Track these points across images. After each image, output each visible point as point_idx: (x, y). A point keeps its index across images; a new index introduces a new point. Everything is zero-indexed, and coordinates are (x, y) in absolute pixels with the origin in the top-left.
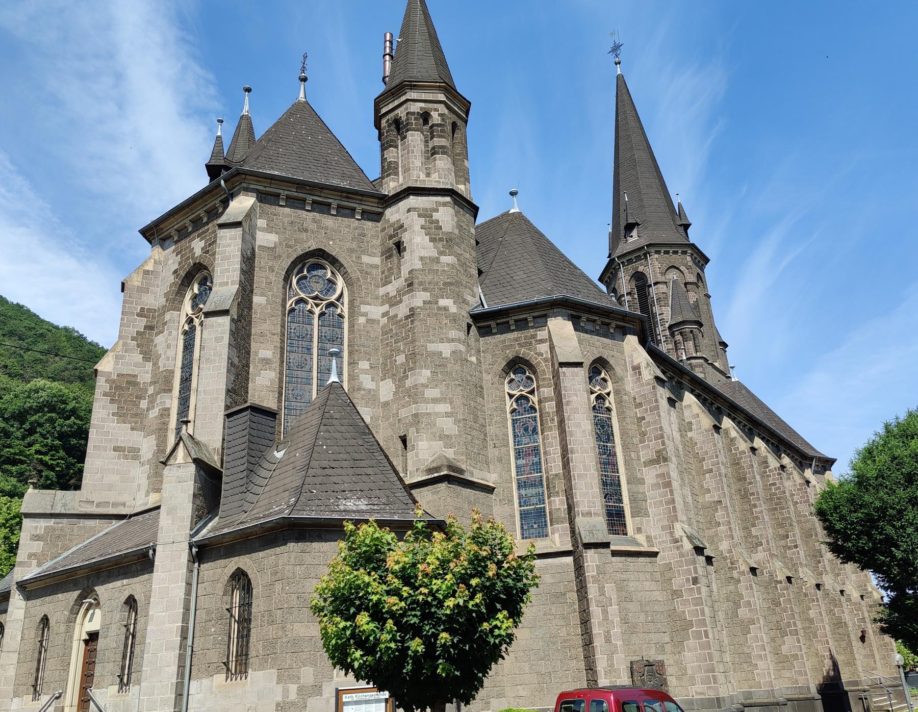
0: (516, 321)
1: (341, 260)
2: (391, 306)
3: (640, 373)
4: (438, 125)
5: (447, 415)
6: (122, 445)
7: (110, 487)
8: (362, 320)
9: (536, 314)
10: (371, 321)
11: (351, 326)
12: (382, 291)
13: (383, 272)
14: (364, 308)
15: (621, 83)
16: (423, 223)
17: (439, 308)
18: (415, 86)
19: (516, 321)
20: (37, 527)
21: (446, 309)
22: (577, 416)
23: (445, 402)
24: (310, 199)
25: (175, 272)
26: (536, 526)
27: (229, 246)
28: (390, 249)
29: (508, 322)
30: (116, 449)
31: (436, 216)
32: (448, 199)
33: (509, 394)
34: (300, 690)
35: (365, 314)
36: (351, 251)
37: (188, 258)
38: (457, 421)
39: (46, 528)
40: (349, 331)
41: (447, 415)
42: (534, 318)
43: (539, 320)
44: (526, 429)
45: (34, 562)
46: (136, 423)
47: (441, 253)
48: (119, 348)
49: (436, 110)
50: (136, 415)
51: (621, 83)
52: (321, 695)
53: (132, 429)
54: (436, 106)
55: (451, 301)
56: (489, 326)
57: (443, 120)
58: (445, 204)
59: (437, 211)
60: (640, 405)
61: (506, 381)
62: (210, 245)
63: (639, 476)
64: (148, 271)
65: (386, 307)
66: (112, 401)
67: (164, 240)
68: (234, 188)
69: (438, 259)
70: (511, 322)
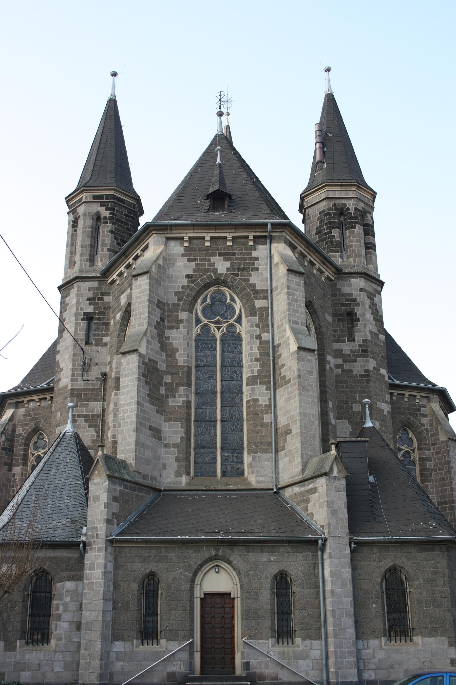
0: (410, 395)
9: (423, 395)
12: (335, 346)
18: (360, 188)
21: (383, 376)
25: (188, 276)
27: (296, 290)
28: (341, 315)
30: (151, 428)
37: (208, 270)
39: (120, 490)
45: (115, 521)
66: (147, 383)
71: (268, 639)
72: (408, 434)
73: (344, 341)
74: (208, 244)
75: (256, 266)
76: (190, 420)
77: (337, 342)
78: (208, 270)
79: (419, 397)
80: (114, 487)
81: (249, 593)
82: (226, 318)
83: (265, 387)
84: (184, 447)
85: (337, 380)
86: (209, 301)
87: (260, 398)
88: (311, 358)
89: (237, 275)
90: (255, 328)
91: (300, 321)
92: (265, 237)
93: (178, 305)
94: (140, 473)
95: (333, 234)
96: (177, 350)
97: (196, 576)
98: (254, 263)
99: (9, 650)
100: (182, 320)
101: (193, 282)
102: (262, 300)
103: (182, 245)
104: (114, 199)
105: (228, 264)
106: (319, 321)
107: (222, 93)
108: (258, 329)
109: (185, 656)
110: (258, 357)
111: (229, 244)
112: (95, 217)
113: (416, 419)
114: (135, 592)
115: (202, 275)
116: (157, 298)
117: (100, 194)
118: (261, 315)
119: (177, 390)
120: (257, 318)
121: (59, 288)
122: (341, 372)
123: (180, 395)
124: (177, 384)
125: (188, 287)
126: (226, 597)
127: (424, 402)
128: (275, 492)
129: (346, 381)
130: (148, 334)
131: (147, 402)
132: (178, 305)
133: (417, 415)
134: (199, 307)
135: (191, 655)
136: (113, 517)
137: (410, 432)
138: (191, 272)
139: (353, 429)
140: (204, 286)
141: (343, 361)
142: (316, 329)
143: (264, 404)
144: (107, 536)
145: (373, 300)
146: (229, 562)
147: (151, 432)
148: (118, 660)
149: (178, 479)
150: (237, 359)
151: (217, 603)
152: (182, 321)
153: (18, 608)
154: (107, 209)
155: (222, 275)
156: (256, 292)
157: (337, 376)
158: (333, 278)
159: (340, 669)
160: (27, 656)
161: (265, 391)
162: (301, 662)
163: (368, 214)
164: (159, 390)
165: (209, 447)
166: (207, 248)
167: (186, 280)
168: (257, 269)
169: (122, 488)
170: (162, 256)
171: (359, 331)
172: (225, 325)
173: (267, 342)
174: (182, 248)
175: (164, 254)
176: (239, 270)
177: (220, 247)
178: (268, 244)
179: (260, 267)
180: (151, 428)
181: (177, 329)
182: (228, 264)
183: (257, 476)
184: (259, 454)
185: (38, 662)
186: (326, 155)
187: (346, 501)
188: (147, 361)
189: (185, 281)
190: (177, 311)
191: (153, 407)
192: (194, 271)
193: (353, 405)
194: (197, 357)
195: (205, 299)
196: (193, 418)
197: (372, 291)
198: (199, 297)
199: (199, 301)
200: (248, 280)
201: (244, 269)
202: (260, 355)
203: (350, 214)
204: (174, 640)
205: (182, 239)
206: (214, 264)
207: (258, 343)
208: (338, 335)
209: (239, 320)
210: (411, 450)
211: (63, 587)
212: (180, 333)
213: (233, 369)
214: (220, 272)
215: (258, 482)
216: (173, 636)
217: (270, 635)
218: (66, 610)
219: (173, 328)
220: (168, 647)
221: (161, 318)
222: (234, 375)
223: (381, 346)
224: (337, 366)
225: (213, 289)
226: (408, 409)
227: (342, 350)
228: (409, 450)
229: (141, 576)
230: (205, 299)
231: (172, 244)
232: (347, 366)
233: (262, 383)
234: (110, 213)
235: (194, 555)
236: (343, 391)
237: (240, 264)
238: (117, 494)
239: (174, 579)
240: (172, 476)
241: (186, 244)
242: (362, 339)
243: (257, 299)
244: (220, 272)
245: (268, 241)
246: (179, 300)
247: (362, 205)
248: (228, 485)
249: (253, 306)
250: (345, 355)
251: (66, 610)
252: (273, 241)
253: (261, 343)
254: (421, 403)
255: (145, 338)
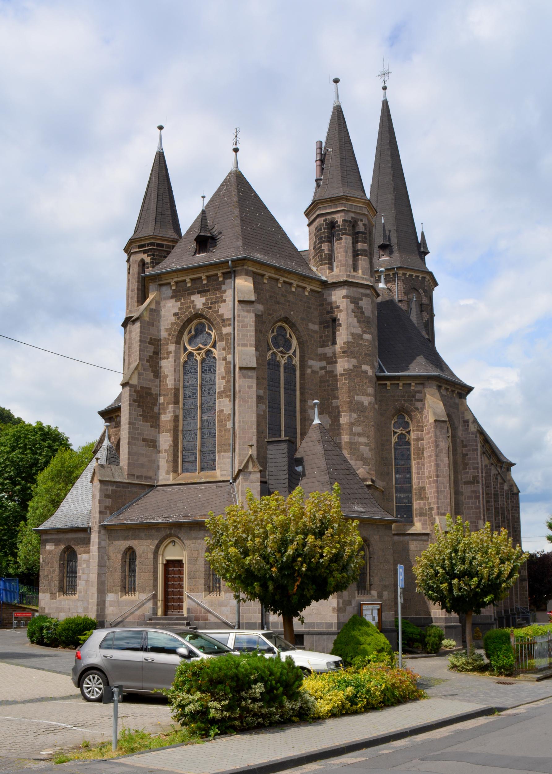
0: (403, 384)
1: (297, 325)
2: (328, 363)
3: (468, 426)
4: (362, 233)
5: (366, 444)
6: (147, 438)
7: (142, 466)
8: (309, 371)
9: (417, 382)
10: (313, 372)
11: (302, 375)
12: (320, 351)
13: (321, 337)
14: (311, 362)
15: (385, 104)
16: (353, 308)
17: (362, 372)
18: (349, 199)
19: (403, 384)
20: (107, 489)
21: (366, 372)
22: (442, 454)
23: (364, 437)
24: (282, 279)
25: (175, 314)
26: (405, 516)
27: (246, 317)
28: (327, 322)
29: (398, 384)
30: (144, 440)
31: (361, 303)
32: (368, 292)
33: (393, 431)
34: (344, 602)
35: (311, 367)
36: (303, 319)
37: (189, 307)
38: (371, 450)
39: (112, 490)
40: (300, 378)
41: (366, 444)
42: (416, 384)
43: (418, 386)
44: (403, 455)
45: (108, 512)
46: (153, 422)
47: (364, 332)
48: (140, 368)
49: (362, 221)
50: (152, 417)
51: (385, 104)
52: (351, 605)
53: (152, 427)
54: (361, 217)
55: (369, 367)
56: (386, 384)
57: (366, 229)
58: (366, 295)
59: (361, 300)
60: (466, 446)
61: (393, 422)
62: (211, 303)
63: (461, 490)
64: (152, 309)
65: (323, 364)
66: (139, 406)
67: (161, 285)
68: (236, 267)
69: (362, 336)
70: (401, 384)
71: (202, 592)
72: (405, 418)
73: (328, 346)
74: (189, 285)
75: (224, 298)
76: (178, 430)
77: (322, 347)
78: (189, 307)
79: (413, 384)
80: (106, 488)
81: (193, 560)
82: (206, 345)
83: (228, 399)
84: (172, 451)
85: (320, 381)
86: (193, 332)
87: (224, 409)
88: (251, 374)
89: (210, 308)
90: (222, 351)
91: (248, 343)
92: (230, 272)
93: (168, 339)
94: (134, 475)
95: (323, 248)
96: (167, 376)
97: (159, 548)
98: (222, 296)
99: (53, 599)
100: (171, 351)
101: (178, 318)
102: (228, 327)
103: (171, 289)
104: (154, 246)
105: (203, 300)
106: (299, 332)
107: (238, 130)
108: (224, 352)
109: (150, 604)
110: (224, 375)
111: (205, 282)
112: (141, 264)
113: (410, 404)
114: (120, 561)
115: (185, 312)
116: (149, 337)
117: (143, 243)
118: (227, 340)
119: (167, 408)
120: (224, 342)
121: (123, 325)
122: (324, 373)
123: (169, 412)
124: (167, 403)
125: (175, 323)
126: (179, 563)
127: (419, 388)
128: (231, 483)
129: (328, 381)
130: (140, 368)
131: (140, 421)
132: (168, 339)
133: (412, 401)
134: (185, 338)
135: (155, 604)
136: (105, 509)
137: (406, 416)
138: (177, 311)
139: (332, 422)
140: (187, 320)
141: (327, 363)
142: (297, 339)
143: (227, 413)
144: (100, 523)
145: (358, 304)
146: (179, 538)
147: (144, 443)
148: (110, 606)
149: (168, 476)
150: (213, 378)
151: (173, 566)
152: (170, 352)
153: (57, 572)
154: (148, 256)
155: (199, 309)
156: (223, 320)
157: (321, 377)
158: (320, 290)
159: (245, 613)
160: (63, 603)
161: (228, 403)
162: (223, 608)
163: (359, 223)
164: (153, 410)
165: (192, 450)
166: (188, 289)
167: (173, 318)
168: (225, 301)
169: (114, 488)
170: (154, 301)
171: (341, 335)
172: (203, 351)
173: (230, 362)
174: (171, 291)
175: (157, 299)
176: (211, 303)
177: (198, 286)
178: (233, 278)
179: (227, 299)
180: (144, 440)
181: (168, 359)
182: (203, 300)
183: (221, 471)
184: (223, 453)
185: (68, 607)
186: (324, 171)
187: (259, 490)
188: (139, 389)
189: (173, 319)
190: (168, 344)
191: (147, 423)
192: (180, 309)
193: (333, 401)
194: (184, 380)
195: (190, 332)
196: (180, 428)
197: (357, 296)
198: (184, 331)
199: (186, 333)
200: (218, 311)
201: (215, 303)
202: (226, 374)
203: (339, 226)
204: (143, 593)
205: (169, 284)
206: (194, 301)
207: (224, 364)
208: (323, 341)
209: (214, 346)
210: (406, 432)
211: (81, 557)
212: (169, 362)
213: (210, 387)
214: (197, 307)
215: (222, 475)
216: (143, 591)
217: (203, 589)
218: (83, 573)
219: (165, 358)
220: (138, 597)
221: (154, 353)
222: (210, 391)
223: (365, 345)
224: (322, 368)
225: (195, 322)
226: (403, 396)
227: (326, 354)
228: (403, 432)
229: (123, 550)
230: (190, 332)
231: (164, 289)
232: (329, 368)
233: (226, 397)
234: (151, 259)
235: (156, 533)
236: (325, 390)
237: (212, 299)
238: (109, 492)
239: (143, 551)
240: (164, 474)
241: (174, 288)
242: (342, 342)
243: (224, 327)
244: (197, 307)
245: (233, 275)
246: (169, 335)
247: (353, 215)
248: (201, 478)
249: (221, 333)
250: (328, 358)
251: (83, 573)
252: (236, 275)
253: (226, 364)
254: (416, 389)
255: (136, 372)
